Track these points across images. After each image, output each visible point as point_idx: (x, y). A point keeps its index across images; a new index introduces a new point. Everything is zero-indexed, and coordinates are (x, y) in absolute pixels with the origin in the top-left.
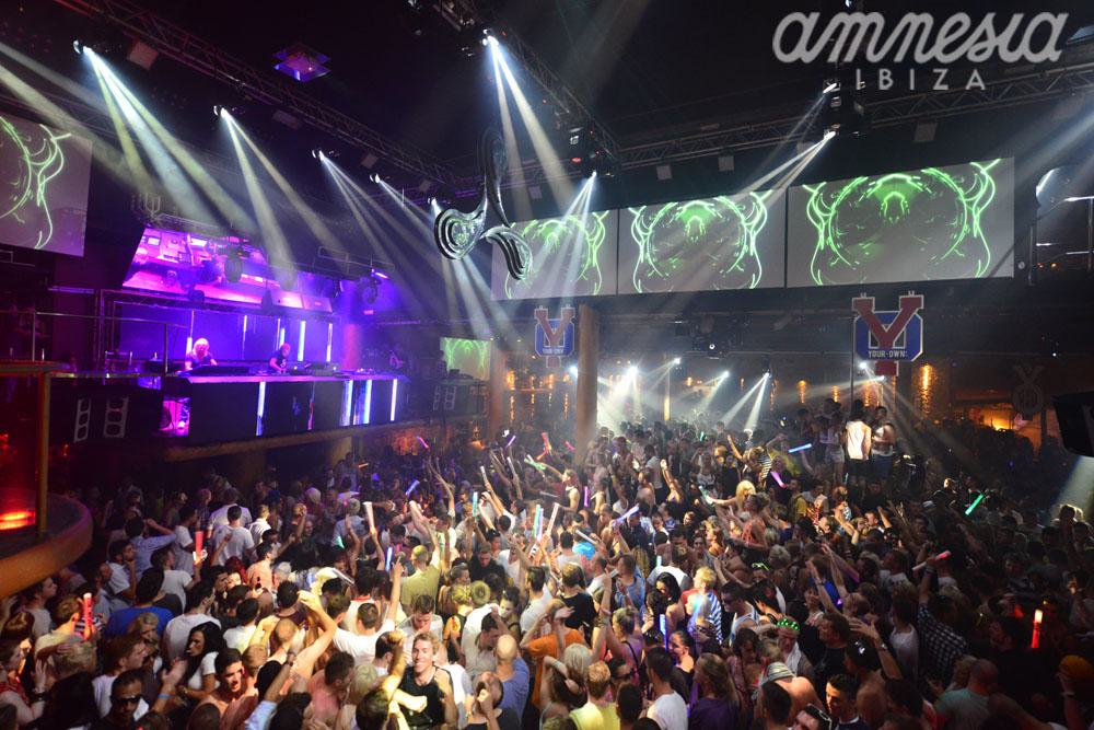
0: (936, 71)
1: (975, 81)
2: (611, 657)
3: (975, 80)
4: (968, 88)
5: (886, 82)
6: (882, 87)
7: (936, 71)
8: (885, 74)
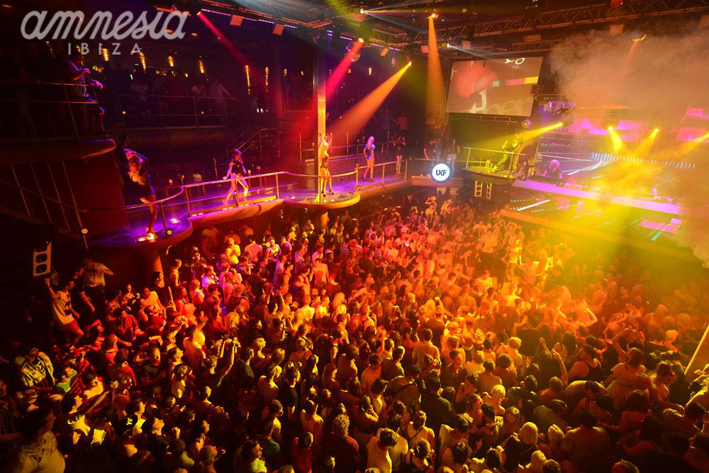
0: (114, 44)
2: (284, 352)
3: (136, 49)
5: (85, 51)
6: (476, 195)
7: (114, 44)
8: (85, 51)
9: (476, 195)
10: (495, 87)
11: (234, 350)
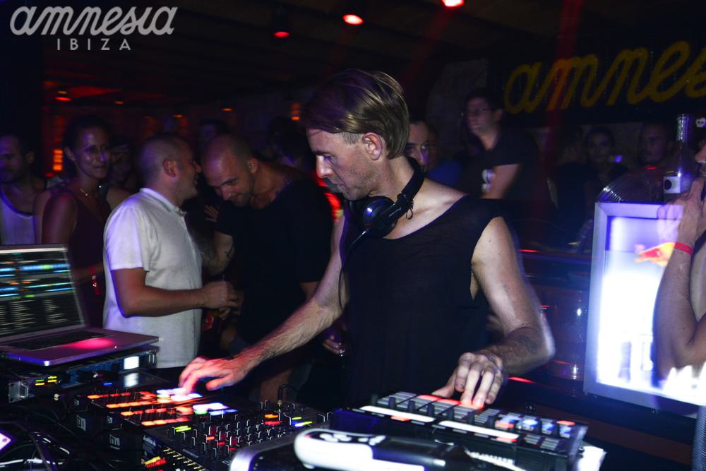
1: (125, 45)
3: (125, 45)
4: (121, 49)
6: (72, 49)
9: (72, 49)
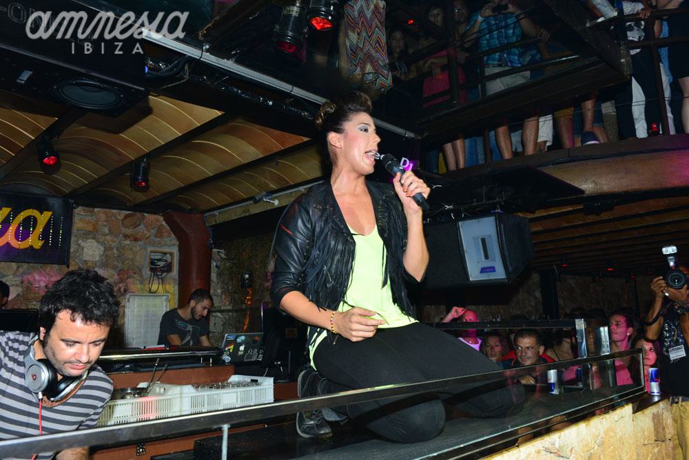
0: (116, 43)
3: (138, 49)
6: (86, 52)
7: (116, 43)
9: (86, 52)
10: (503, 126)
11: (153, 249)
